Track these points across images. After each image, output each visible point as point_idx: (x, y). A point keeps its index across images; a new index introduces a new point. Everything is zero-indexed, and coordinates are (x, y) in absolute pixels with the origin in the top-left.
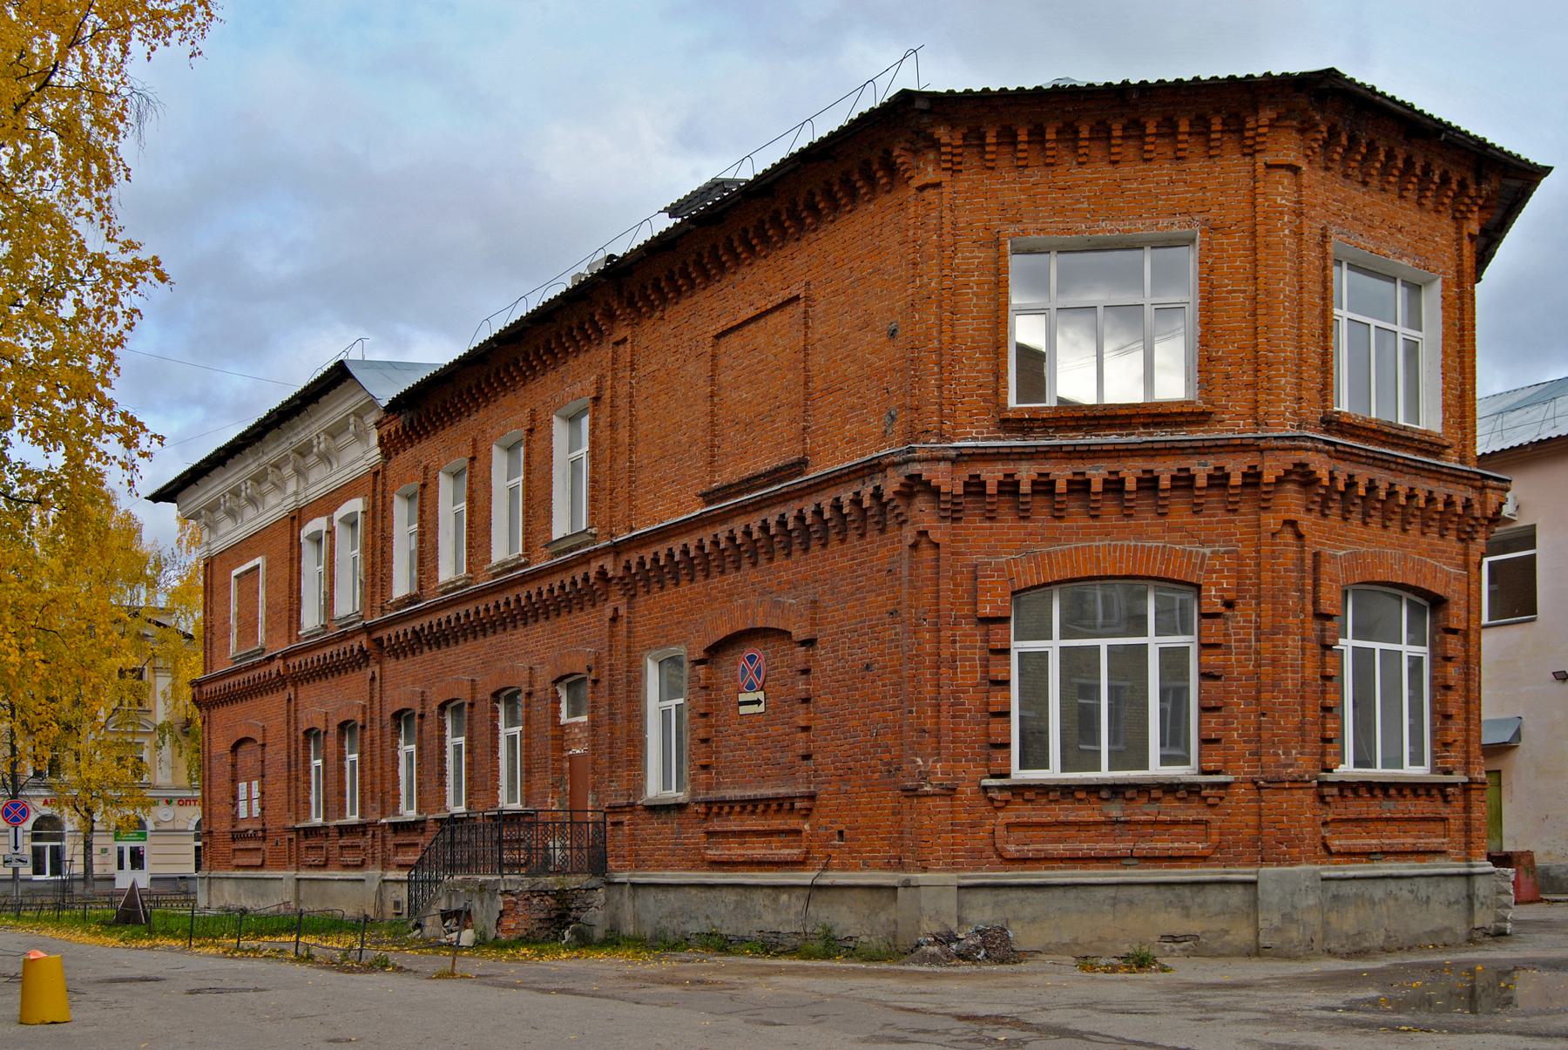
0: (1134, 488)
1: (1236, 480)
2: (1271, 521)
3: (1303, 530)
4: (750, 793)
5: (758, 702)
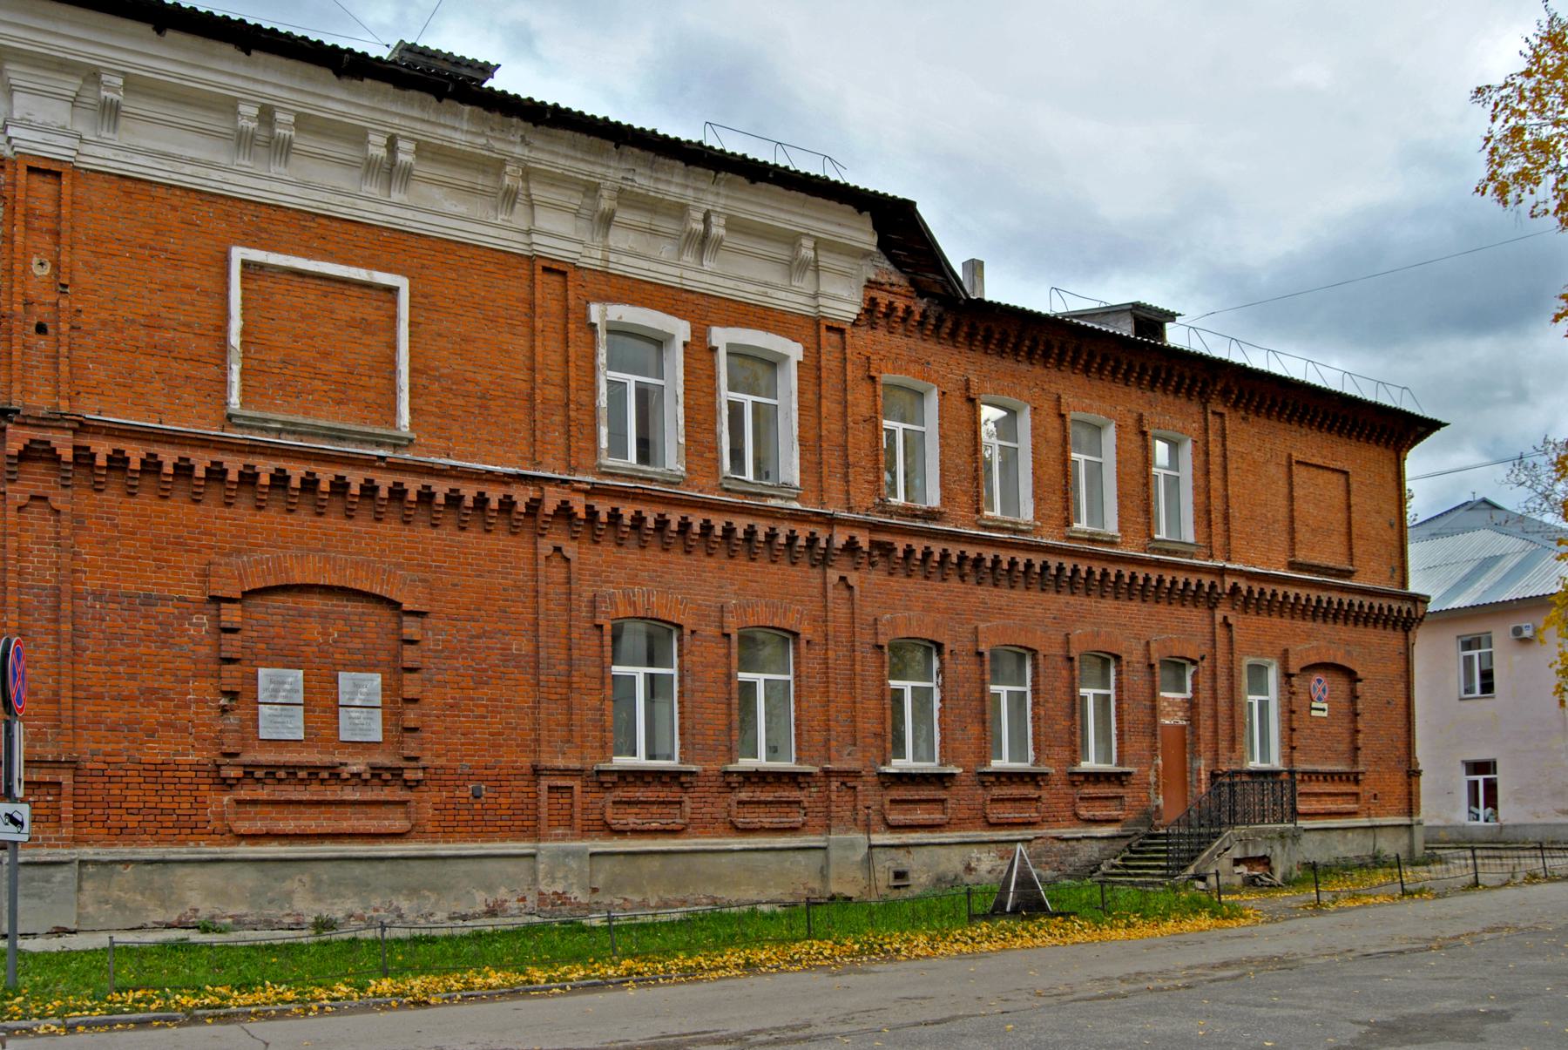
0: (172, 472)
1: (265, 480)
2: (545, 547)
3: (851, 582)
4: (1320, 768)
5: (1323, 710)
